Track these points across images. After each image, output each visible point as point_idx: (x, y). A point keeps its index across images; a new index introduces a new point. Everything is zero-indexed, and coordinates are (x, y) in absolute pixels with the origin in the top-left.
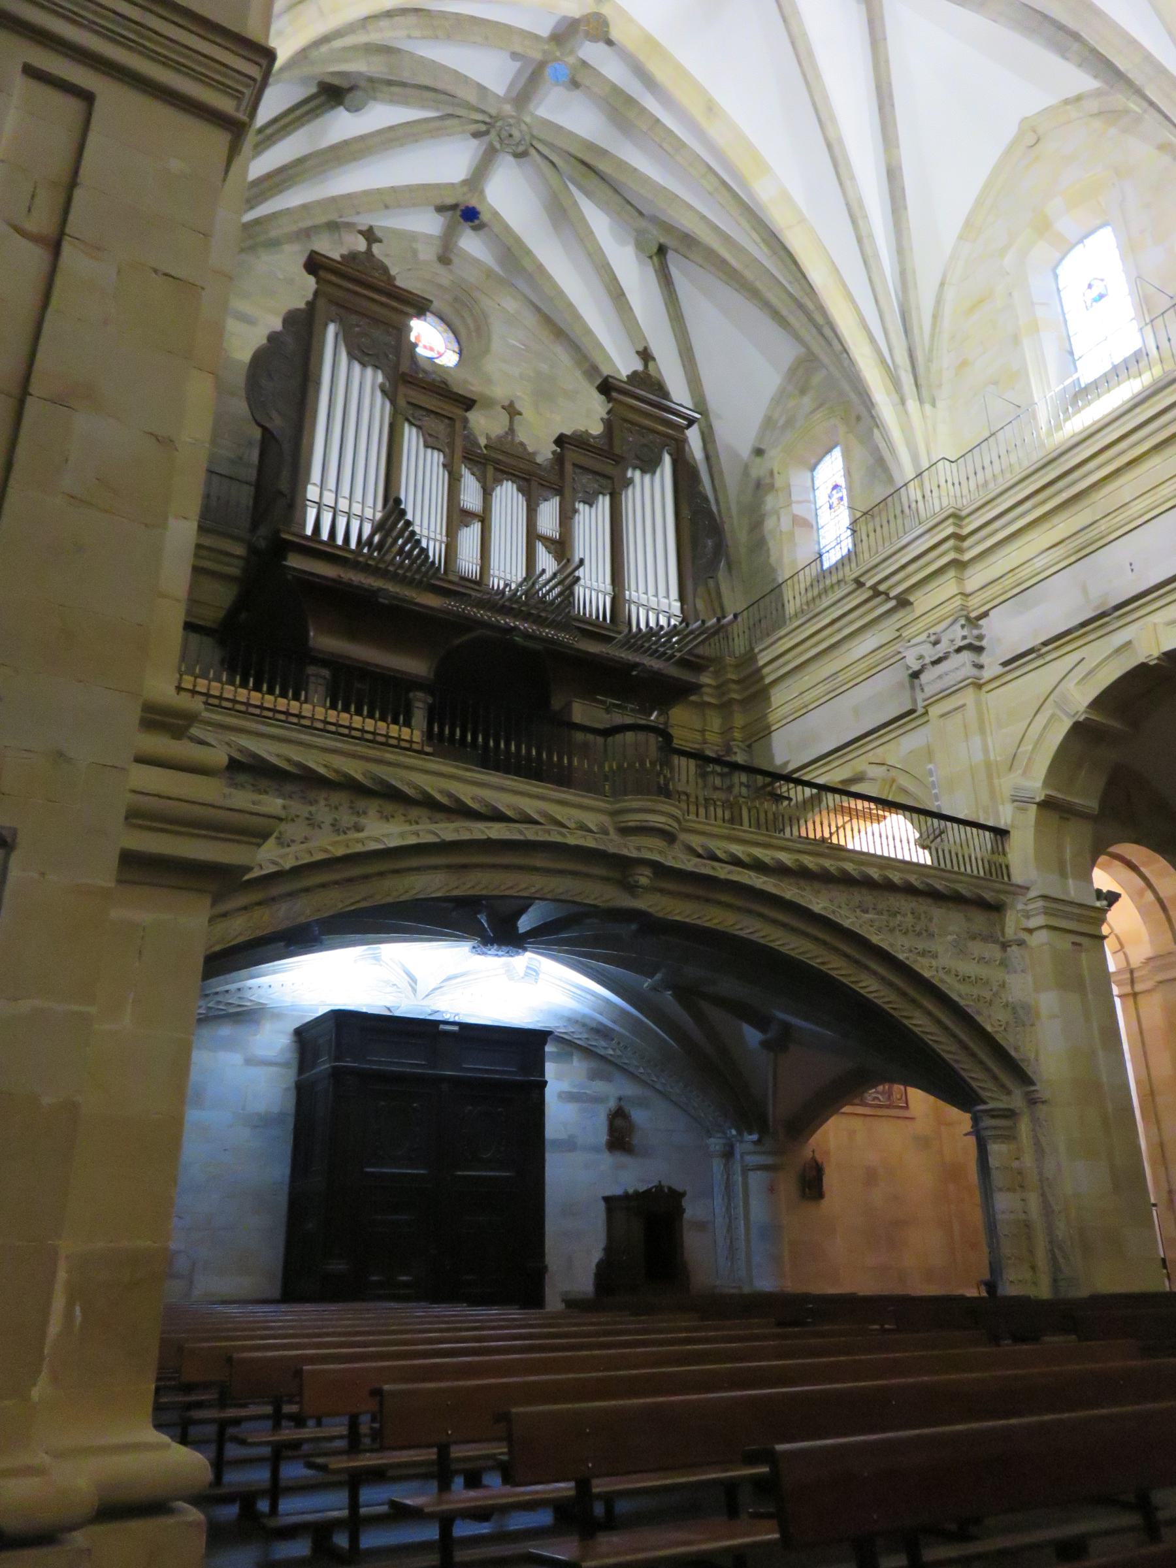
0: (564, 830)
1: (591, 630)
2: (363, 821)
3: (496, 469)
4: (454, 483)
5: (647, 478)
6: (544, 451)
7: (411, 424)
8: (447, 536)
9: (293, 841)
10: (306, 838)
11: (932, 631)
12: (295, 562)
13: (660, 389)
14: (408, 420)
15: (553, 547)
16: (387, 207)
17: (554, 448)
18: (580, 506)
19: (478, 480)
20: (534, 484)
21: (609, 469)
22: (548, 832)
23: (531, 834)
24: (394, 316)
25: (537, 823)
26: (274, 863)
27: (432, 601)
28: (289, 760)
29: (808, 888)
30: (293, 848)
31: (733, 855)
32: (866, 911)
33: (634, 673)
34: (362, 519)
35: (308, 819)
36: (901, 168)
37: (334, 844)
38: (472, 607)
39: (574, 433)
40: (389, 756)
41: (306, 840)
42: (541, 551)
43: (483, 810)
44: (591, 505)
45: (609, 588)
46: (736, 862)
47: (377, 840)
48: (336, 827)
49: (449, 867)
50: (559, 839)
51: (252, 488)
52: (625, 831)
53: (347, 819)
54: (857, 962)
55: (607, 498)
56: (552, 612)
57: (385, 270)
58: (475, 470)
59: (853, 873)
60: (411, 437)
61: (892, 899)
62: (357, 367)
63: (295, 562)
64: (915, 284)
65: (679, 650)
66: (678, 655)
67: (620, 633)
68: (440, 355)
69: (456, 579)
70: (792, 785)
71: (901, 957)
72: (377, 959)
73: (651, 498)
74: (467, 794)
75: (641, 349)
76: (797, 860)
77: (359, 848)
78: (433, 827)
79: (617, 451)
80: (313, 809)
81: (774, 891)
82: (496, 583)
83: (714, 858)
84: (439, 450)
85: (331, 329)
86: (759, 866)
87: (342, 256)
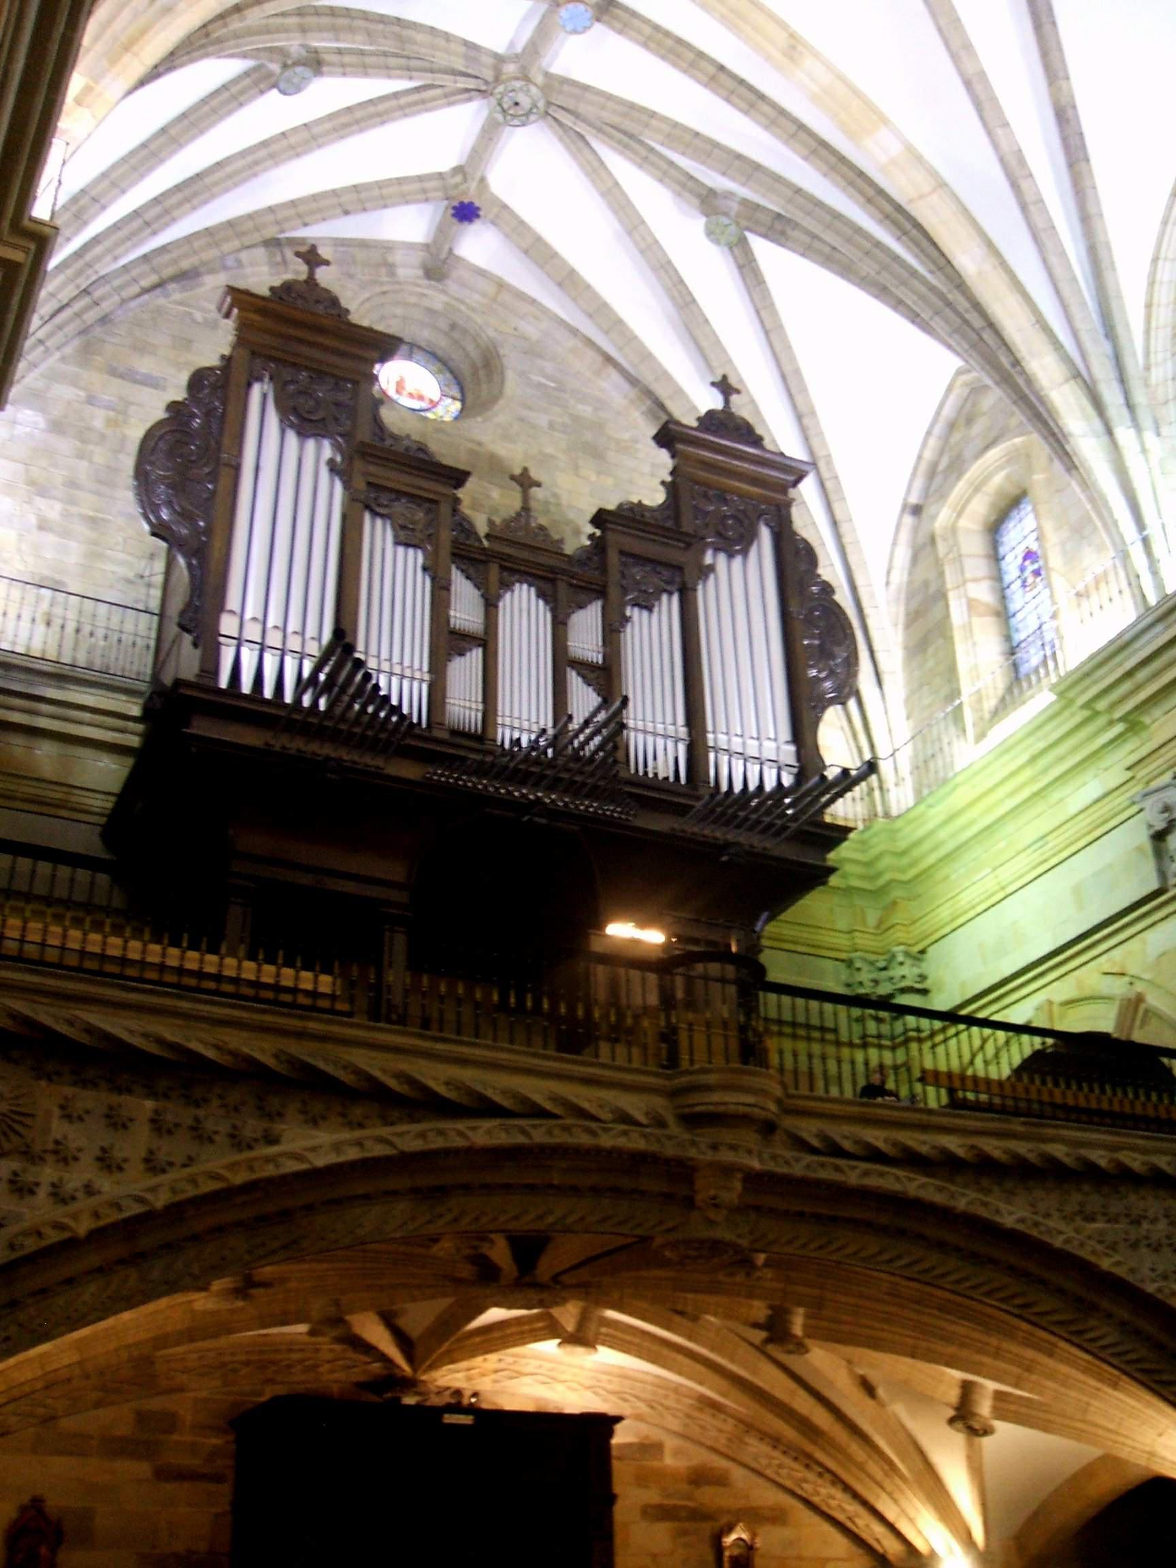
0: (593, 1125)
1: (651, 794)
2: (279, 1127)
3: (503, 568)
5: (737, 561)
6: (578, 536)
7: (375, 514)
8: (430, 671)
9: (171, 1164)
10: (190, 1158)
13: (747, 433)
14: (367, 507)
15: (592, 676)
16: (346, 213)
17: (590, 529)
18: (633, 613)
19: (477, 586)
20: (562, 587)
21: (676, 555)
22: (566, 1129)
23: (540, 1133)
24: (348, 363)
25: (556, 1117)
26: (140, 1200)
27: (409, 771)
28: (160, 1041)
29: (996, 1189)
30: (172, 1175)
31: (869, 1146)
32: (1091, 1218)
33: (724, 858)
34: (302, 656)
35: (193, 1129)
36: (1074, 107)
37: (232, 1167)
38: (469, 774)
39: (620, 506)
40: (313, 1026)
41: (190, 1161)
42: (575, 681)
43: (465, 1100)
44: (650, 609)
45: (683, 732)
46: (874, 1155)
47: (297, 1157)
48: (237, 1141)
49: (415, 1191)
50: (585, 1140)
51: (156, 618)
52: (693, 1120)
53: (252, 1126)
55: (675, 599)
56: (592, 775)
57: (334, 302)
58: (471, 571)
59: (1067, 1160)
61: (1133, 1198)
62: (292, 438)
63: (202, 727)
64: (1112, 263)
65: (794, 818)
66: (794, 825)
67: (698, 798)
68: (434, 404)
69: (444, 735)
70: (962, 1027)
71: (1150, 1288)
74: (437, 1077)
75: (718, 379)
76: (973, 1147)
77: (270, 1171)
78: (384, 1131)
79: (687, 527)
80: (201, 1113)
81: (939, 1198)
82: (504, 735)
83: (836, 1151)
84: (415, 546)
86: (911, 1160)
87: (272, 289)
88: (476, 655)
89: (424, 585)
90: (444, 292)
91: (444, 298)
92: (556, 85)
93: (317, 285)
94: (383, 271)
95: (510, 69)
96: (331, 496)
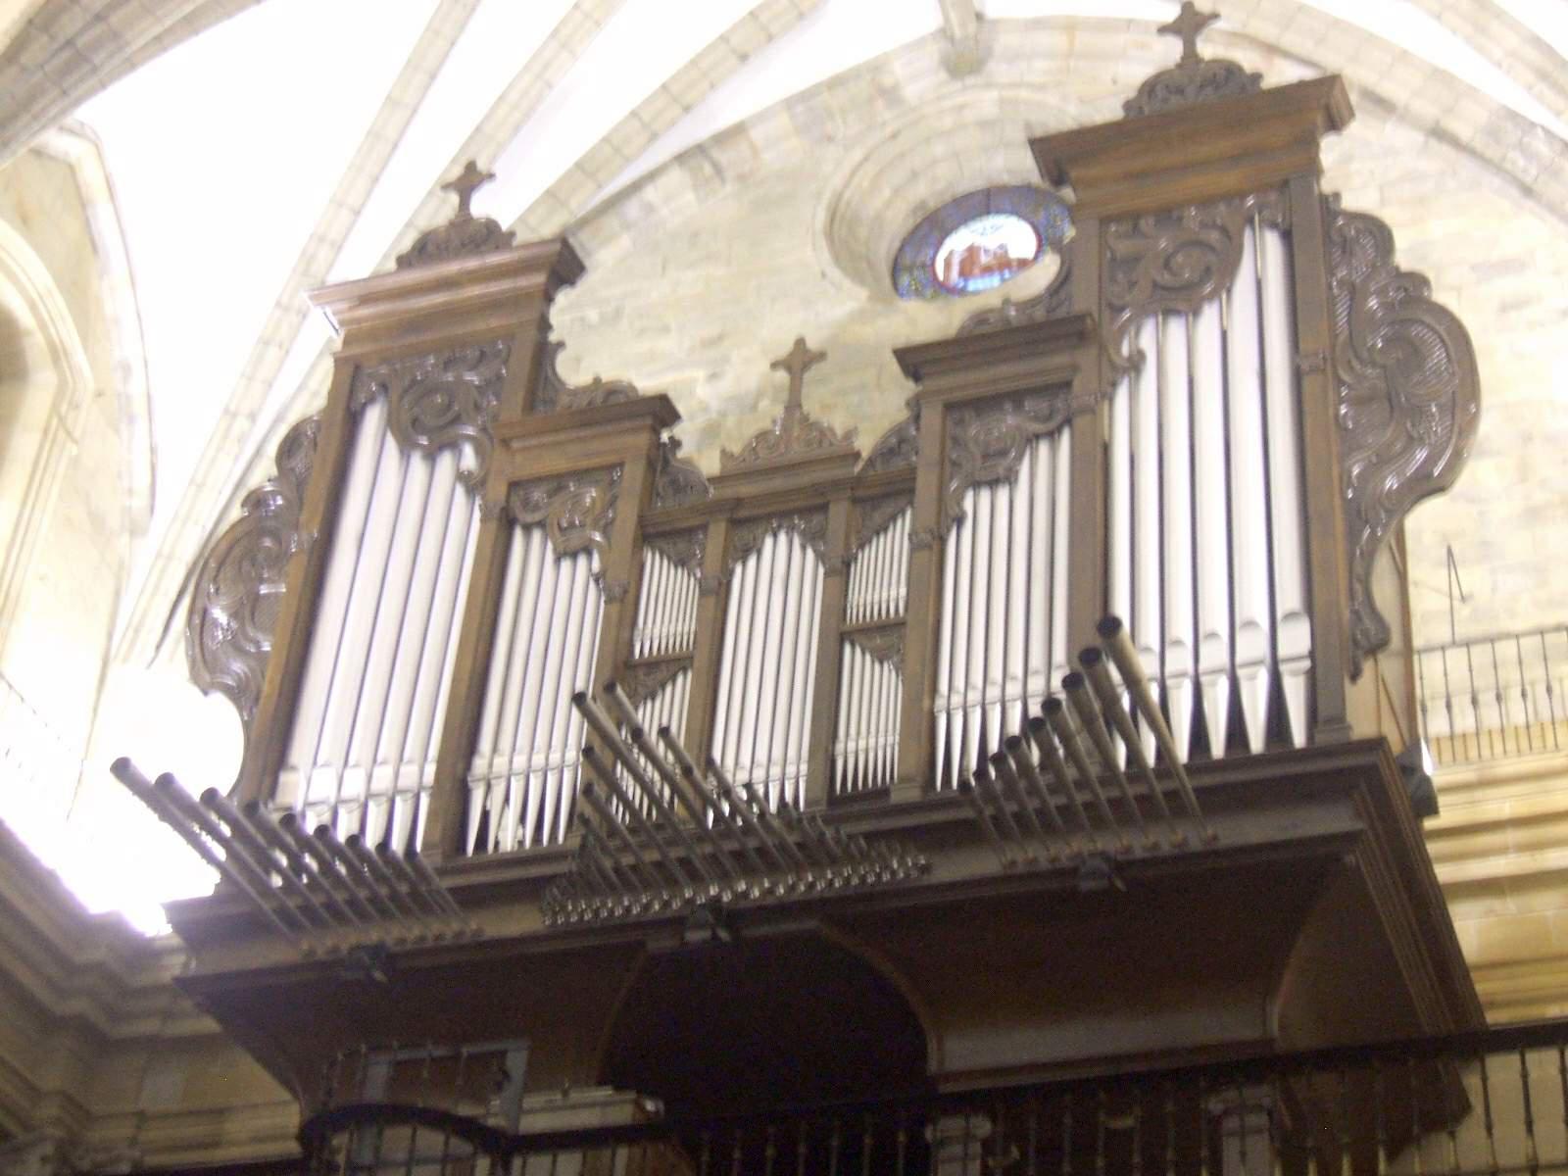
90: (988, 85)
91: (994, 94)
93: (472, 218)
94: (880, 103)
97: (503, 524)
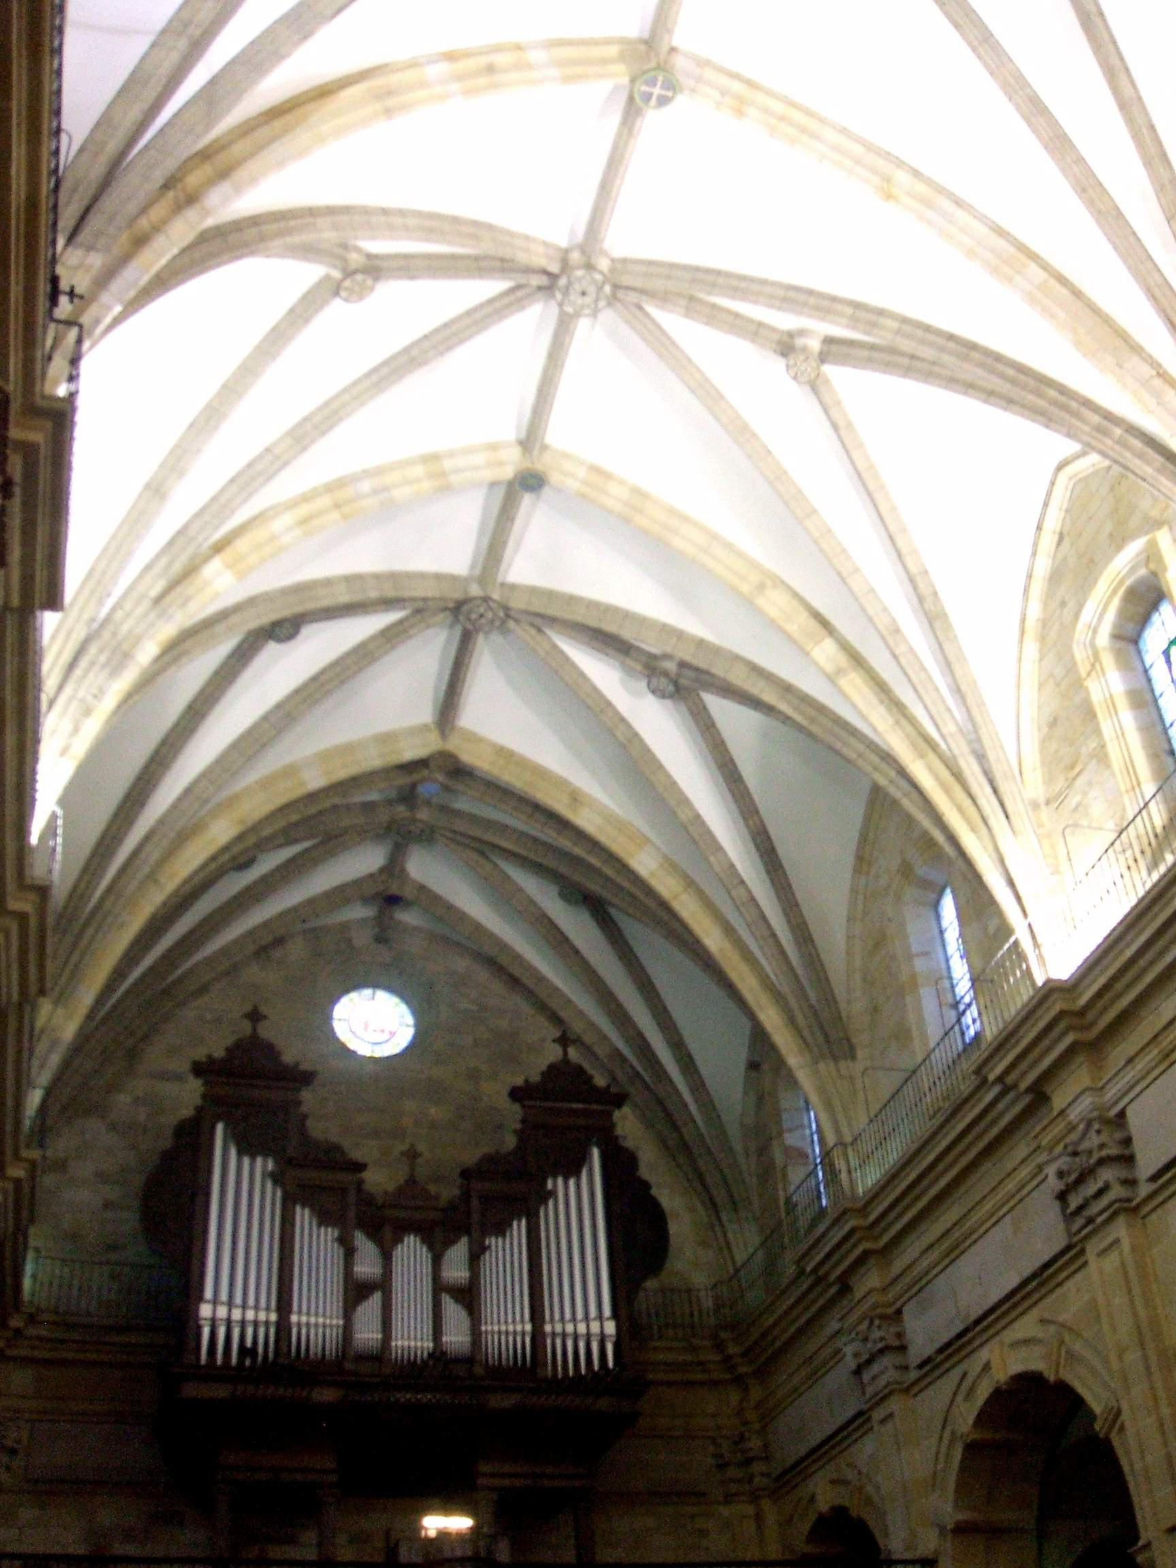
4: (350, 1253)
11: (1067, 1140)
12: (191, 1390)
54: (1148, 1368)
60: (303, 1216)
62: (246, 1161)
72: (1035, 769)
73: (577, 1211)
85: (220, 1128)
88: (377, 1297)
89: (338, 1252)
92: (619, 266)
95: (575, 256)
96: (273, 1195)
97: (289, 1202)
